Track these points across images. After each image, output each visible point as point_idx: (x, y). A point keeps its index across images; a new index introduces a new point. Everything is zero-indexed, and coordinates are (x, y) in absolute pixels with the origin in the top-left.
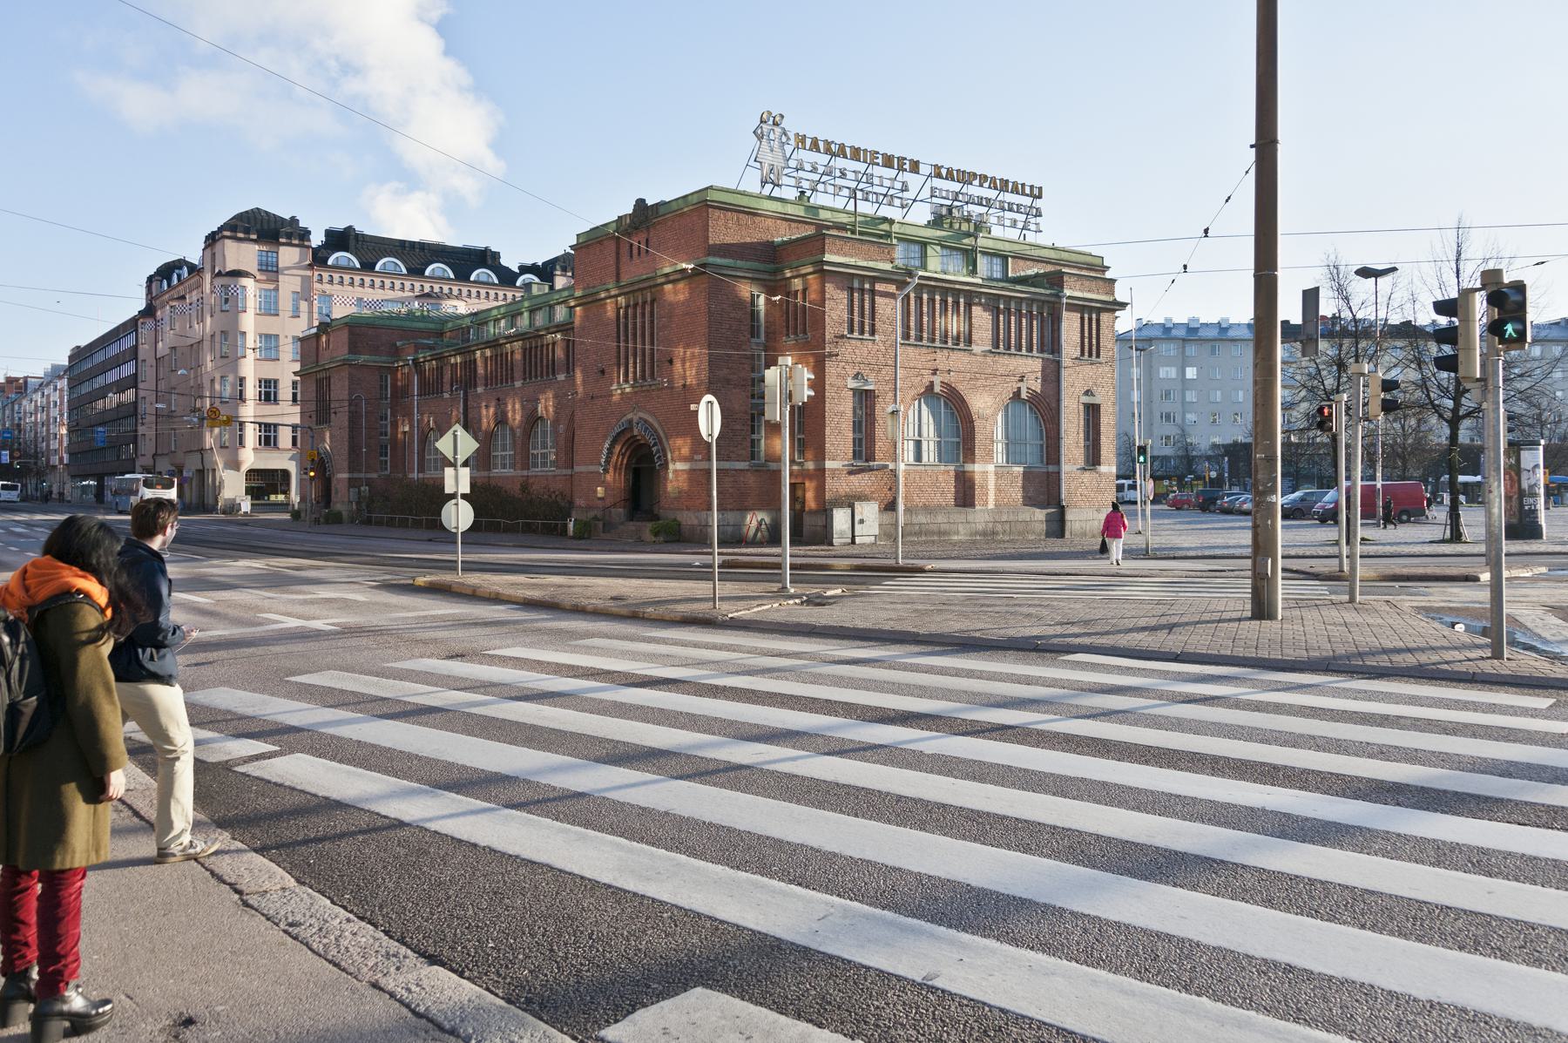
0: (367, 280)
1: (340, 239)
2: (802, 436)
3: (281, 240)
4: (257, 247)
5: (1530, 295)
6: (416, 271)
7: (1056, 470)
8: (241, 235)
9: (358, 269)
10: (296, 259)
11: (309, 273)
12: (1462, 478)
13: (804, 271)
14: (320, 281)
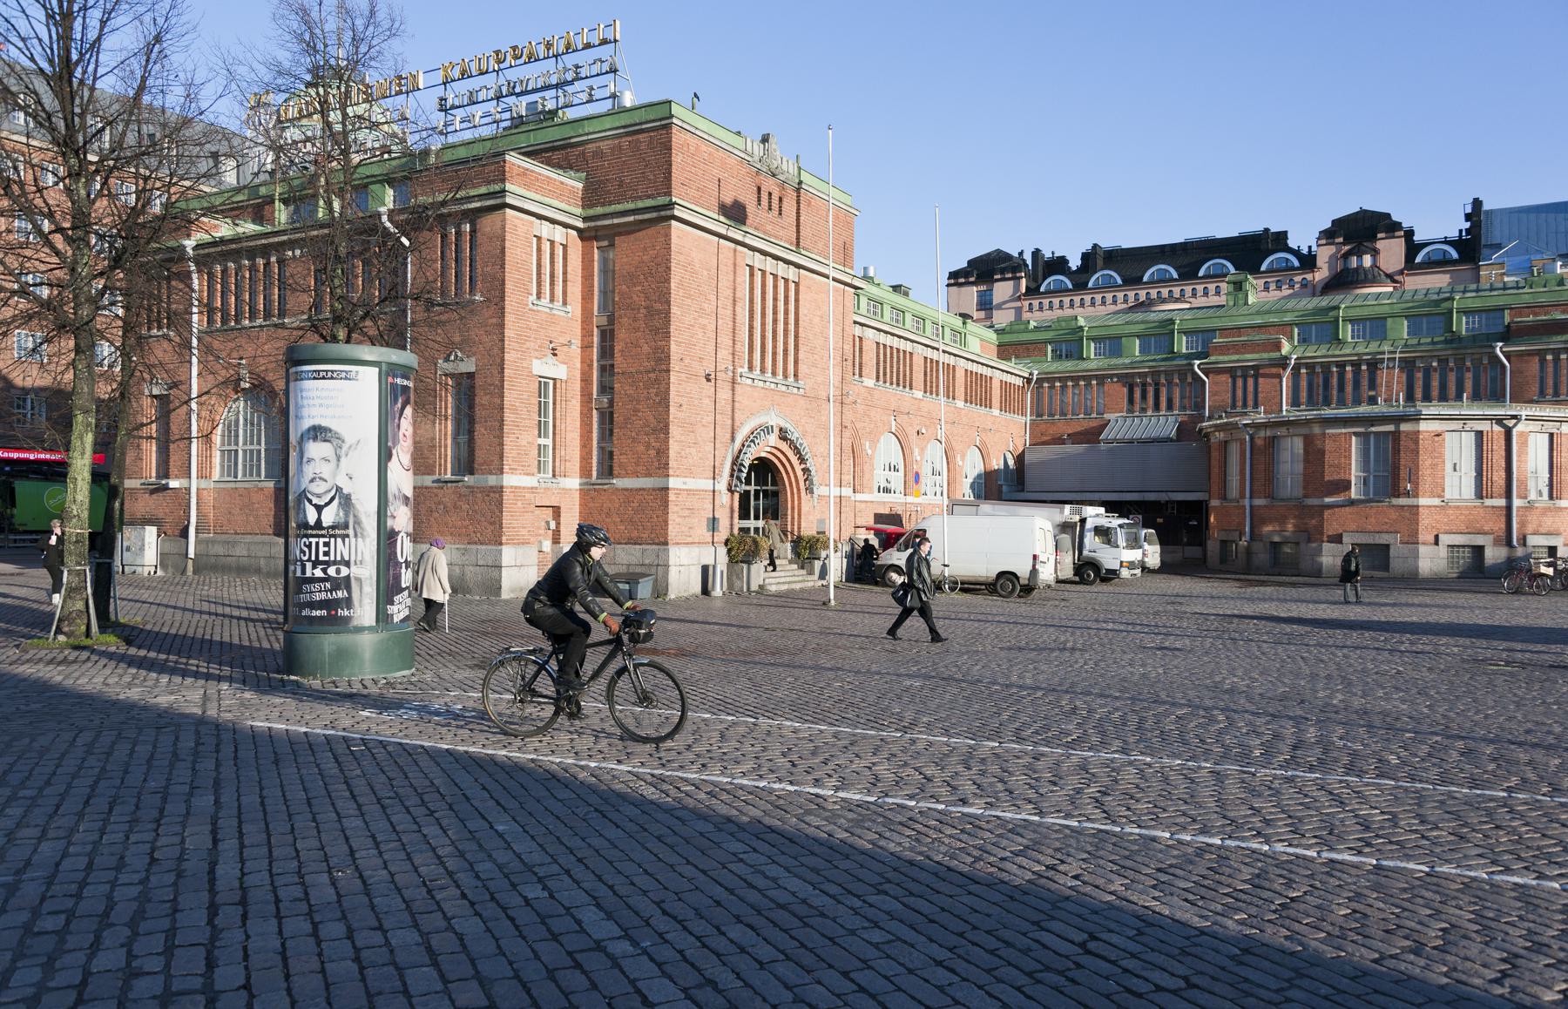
0: (1036, 303)
1: (1092, 259)
2: (542, 441)
3: (1379, 236)
4: (975, 289)
5: (1289, 235)
6: (1133, 281)
7: (186, 485)
8: (962, 280)
9: (1176, 280)
10: (1011, 291)
11: (1018, 304)
12: (1296, 330)
13: (1338, 240)
14: (1031, 309)
